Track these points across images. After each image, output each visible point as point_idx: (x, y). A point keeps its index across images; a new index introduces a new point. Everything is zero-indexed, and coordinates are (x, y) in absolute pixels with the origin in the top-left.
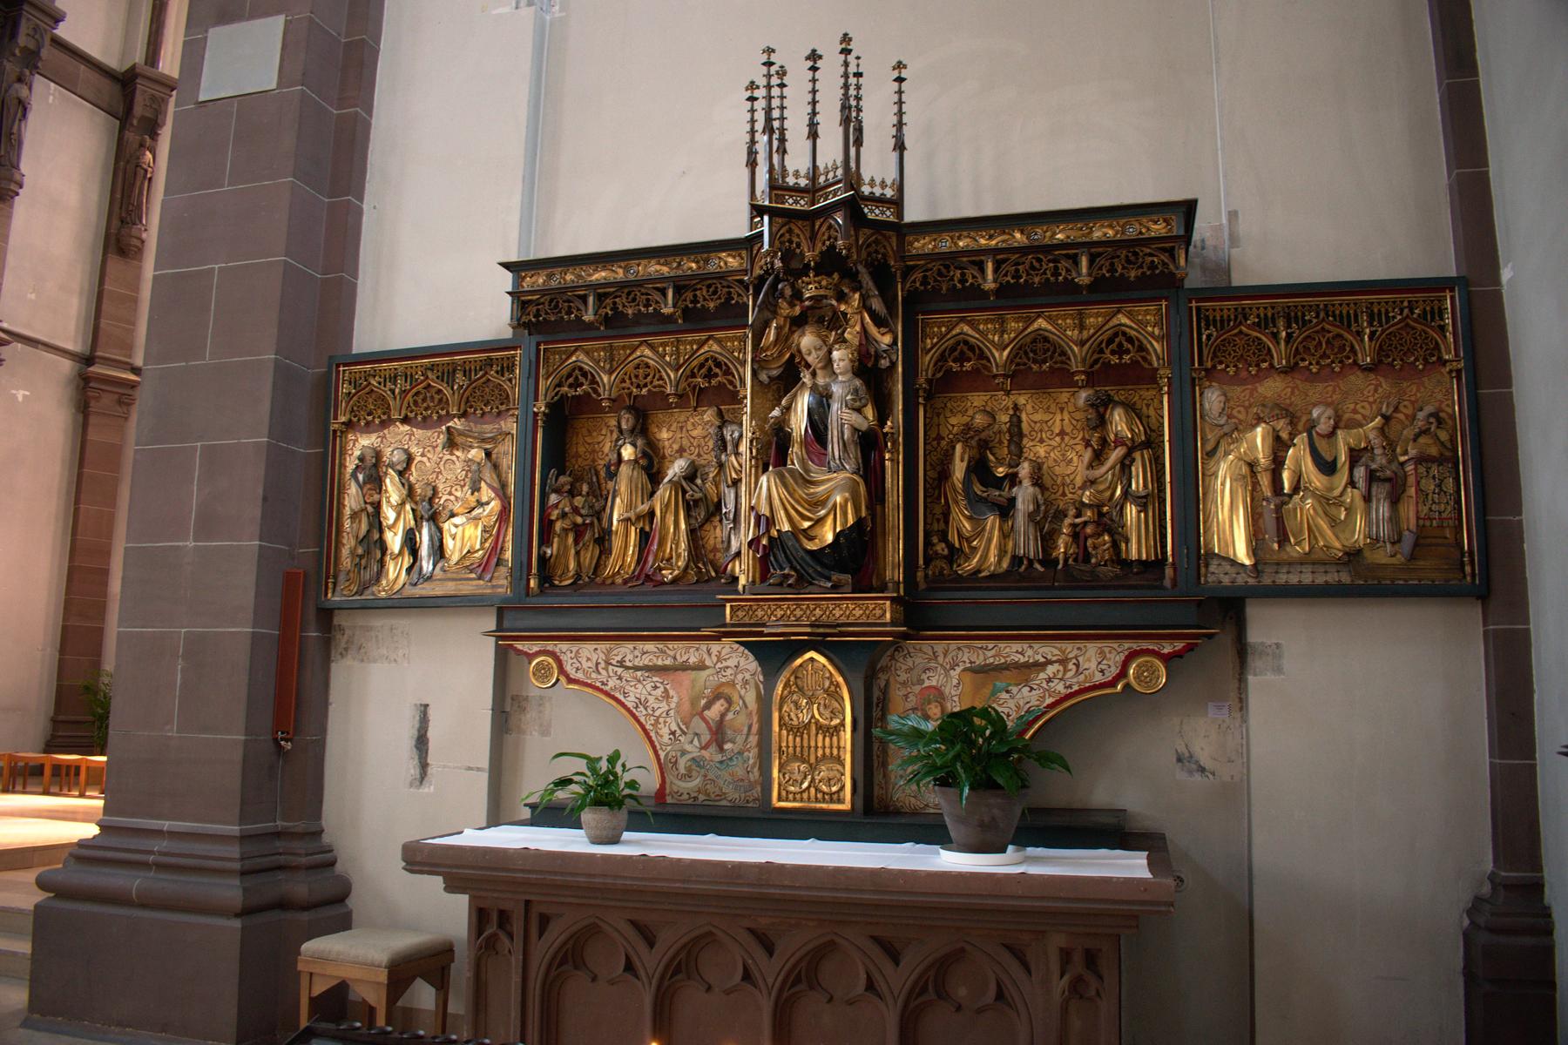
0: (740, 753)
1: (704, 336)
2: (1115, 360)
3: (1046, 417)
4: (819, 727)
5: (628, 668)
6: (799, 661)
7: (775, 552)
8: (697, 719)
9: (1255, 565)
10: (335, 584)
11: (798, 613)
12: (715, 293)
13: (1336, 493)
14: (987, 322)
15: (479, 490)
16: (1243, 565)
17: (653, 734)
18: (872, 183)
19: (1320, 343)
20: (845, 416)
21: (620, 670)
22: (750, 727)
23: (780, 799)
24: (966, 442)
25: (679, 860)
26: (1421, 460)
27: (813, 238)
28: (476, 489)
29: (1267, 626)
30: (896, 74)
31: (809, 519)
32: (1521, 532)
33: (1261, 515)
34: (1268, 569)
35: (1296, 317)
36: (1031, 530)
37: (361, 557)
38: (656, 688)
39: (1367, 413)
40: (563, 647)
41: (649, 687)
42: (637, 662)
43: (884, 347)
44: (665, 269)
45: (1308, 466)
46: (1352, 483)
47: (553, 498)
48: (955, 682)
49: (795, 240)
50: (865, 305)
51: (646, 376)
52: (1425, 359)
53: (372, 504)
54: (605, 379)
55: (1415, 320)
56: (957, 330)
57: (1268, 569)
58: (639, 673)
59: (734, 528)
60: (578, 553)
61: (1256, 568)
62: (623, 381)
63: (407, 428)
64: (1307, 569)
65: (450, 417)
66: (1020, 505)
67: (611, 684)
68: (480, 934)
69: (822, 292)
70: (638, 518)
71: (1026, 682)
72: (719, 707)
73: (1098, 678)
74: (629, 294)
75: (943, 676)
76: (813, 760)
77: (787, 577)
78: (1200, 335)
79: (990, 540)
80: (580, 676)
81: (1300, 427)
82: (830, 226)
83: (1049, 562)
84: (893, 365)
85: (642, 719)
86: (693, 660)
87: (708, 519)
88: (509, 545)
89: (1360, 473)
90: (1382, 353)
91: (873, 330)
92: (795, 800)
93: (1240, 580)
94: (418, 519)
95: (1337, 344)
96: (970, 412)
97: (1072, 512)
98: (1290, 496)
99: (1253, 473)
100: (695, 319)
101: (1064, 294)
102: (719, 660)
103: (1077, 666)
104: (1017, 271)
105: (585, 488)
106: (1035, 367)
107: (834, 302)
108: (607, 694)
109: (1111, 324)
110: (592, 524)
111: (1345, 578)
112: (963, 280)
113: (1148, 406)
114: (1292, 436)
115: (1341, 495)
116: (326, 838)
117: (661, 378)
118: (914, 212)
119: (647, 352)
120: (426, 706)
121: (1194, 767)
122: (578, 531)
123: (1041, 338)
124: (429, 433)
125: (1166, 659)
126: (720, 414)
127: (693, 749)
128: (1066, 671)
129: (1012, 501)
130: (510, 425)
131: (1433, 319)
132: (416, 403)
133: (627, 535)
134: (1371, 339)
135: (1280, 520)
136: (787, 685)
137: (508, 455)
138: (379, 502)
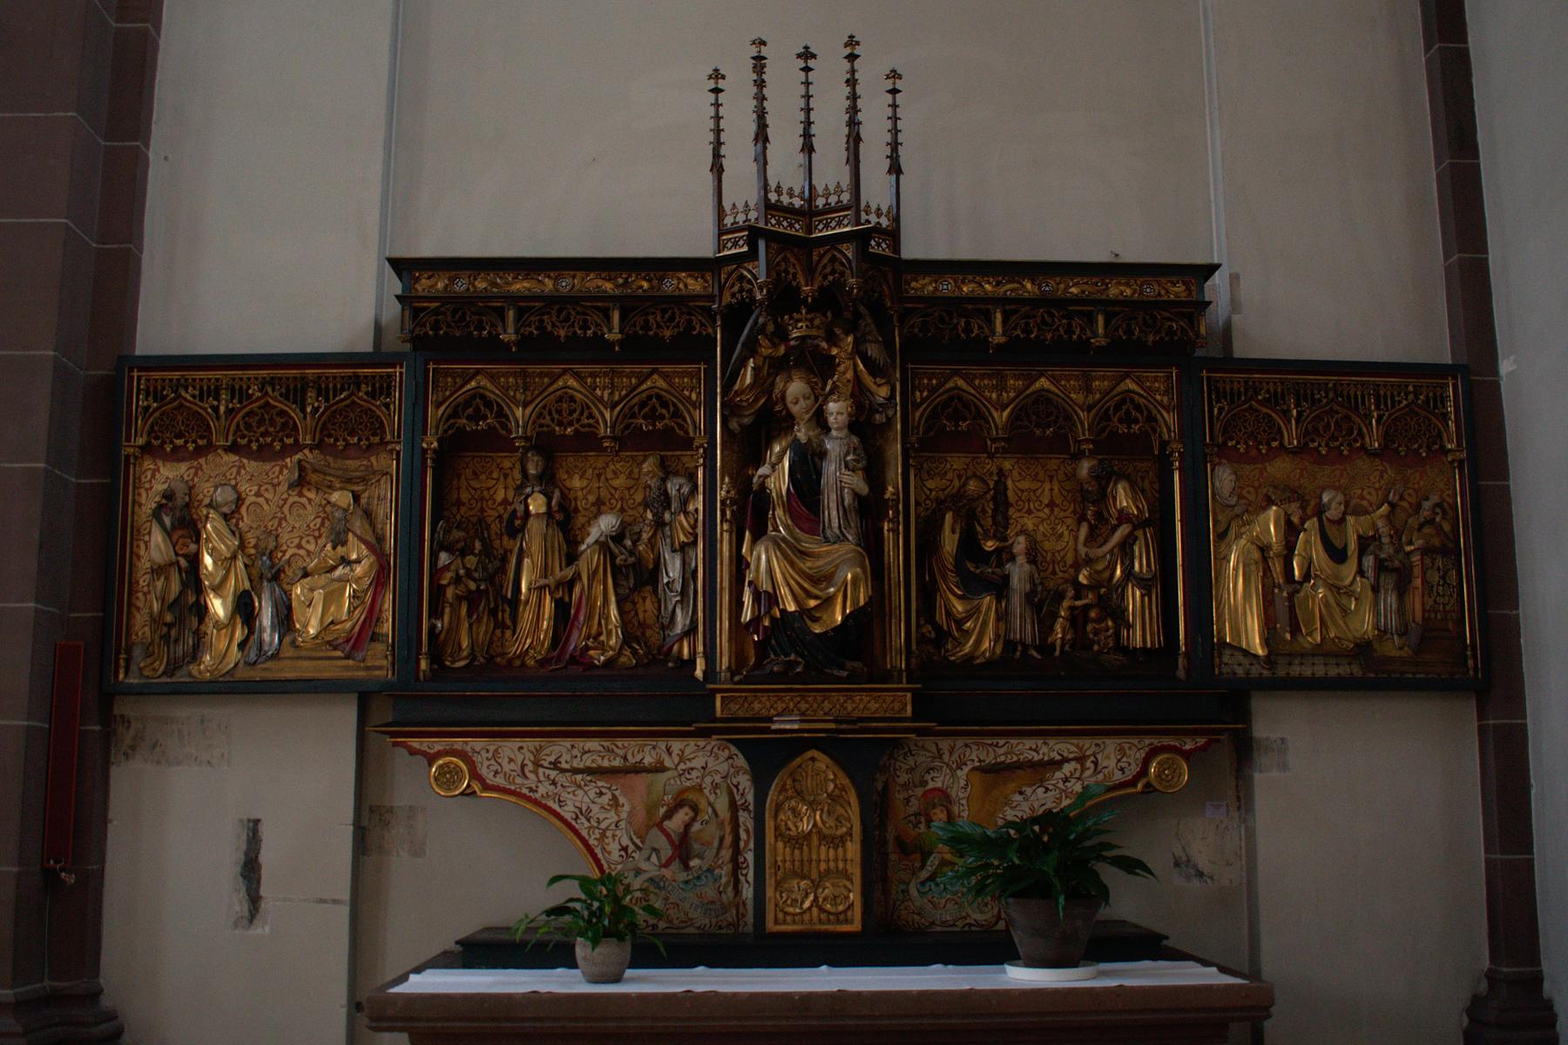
0: (710, 870)
1: (646, 368)
2: (1123, 429)
3: (1034, 486)
4: (823, 838)
5: (563, 771)
6: (799, 760)
8: (655, 830)
10: (128, 661)
11: (804, 706)
12: (672, 319)
13: (1347, 582)
14: (983, 377)
15: (344, 543)
16: (1256, 656)
17: (598, 851)
18: (827, 195)
20: (846, 479)
21: (553, 774)
22: (722, 839)
23: (776, 922)
24: (956, 512)
25: (735, 994)
26: (1426, 551)
27: (810, 271)
28: (340, 541)
29: (1272, 721)
30: (889, 85)
31: (816, 597)
32: (1518, 624)
35: (1305, 395)
36: (1028, 613)
37: (170, 626)
38: (601, 794)
39: (1373, 499)
40: (478, 743)
41: (592, 794)
43: (881, 400)
44: (608, 286)
45: (1318, 554)
46: (1361, 572)
47: (444, 558)
48: (962, 783)
49: (791, 270)
50: (859, 351)
51: (571, 412)
52: (1429, 447)
53: (185, 556)
54: (519, 412)
55: (1419, 407)
56: (950, 384)
58: (579, 777)
59: (681, 602)
60: (471, 625)
61: (1269, 660)
62: (540, 415)
63: (233, 458)
65: (298, 447)
67: (542, 790)
69: (814, 332)
70: (559, 584)
71: (1041, 782)
72: (682, 816)
73: (1118, 777)
74: (560, 311)
75: (955, 778)
76: (814, 875)
78: (1211, 412)
79: (985, 623)
80: (500, 781)
81: (1309, 511)
82: (833, 260)
83: (1045, 648)
84: (890, 421)
85: (584, 833)
86: (648, 760)
87: (636, 588)
89: (1369, 562)
90: (1387, 438)
91: (868, 380)
92: (794, 922)
93: (1255, 671)
94: (256, 581)
96: (950, 476)
97: (1071, 593)
99: (1265, 559)
100: (639, 349)
101: (1078, 355)
102: (682, 759)
103: (1096, 763)
105: (478, 545)
107: (824, 345)
108: (536, 803)
109: (1118, 389)
110: (487, 590)
111: (1357, 671)
112: (968, 330)
113: (1143, 478)
115: (1352, 584)
116: (106, 1002)
117: (591, 416)
118: (913, 248)
119: (572, 382)
120: (257, 822)
121: (1192, 871)
122: (473, 599)
123: (1042, 397)
124: (268, 466)
125: (1186, 755)
126: (663, 464)
127: (651, 868)
128: (1083, 769)
129: (1006, 578)
130: (381, 461)
131: (1436, 407)
132: (248, 427)
133: (540, 605)
134: (1378, 422)
135: (1292, 608)
136: (783, 789)
137: (385, 499)
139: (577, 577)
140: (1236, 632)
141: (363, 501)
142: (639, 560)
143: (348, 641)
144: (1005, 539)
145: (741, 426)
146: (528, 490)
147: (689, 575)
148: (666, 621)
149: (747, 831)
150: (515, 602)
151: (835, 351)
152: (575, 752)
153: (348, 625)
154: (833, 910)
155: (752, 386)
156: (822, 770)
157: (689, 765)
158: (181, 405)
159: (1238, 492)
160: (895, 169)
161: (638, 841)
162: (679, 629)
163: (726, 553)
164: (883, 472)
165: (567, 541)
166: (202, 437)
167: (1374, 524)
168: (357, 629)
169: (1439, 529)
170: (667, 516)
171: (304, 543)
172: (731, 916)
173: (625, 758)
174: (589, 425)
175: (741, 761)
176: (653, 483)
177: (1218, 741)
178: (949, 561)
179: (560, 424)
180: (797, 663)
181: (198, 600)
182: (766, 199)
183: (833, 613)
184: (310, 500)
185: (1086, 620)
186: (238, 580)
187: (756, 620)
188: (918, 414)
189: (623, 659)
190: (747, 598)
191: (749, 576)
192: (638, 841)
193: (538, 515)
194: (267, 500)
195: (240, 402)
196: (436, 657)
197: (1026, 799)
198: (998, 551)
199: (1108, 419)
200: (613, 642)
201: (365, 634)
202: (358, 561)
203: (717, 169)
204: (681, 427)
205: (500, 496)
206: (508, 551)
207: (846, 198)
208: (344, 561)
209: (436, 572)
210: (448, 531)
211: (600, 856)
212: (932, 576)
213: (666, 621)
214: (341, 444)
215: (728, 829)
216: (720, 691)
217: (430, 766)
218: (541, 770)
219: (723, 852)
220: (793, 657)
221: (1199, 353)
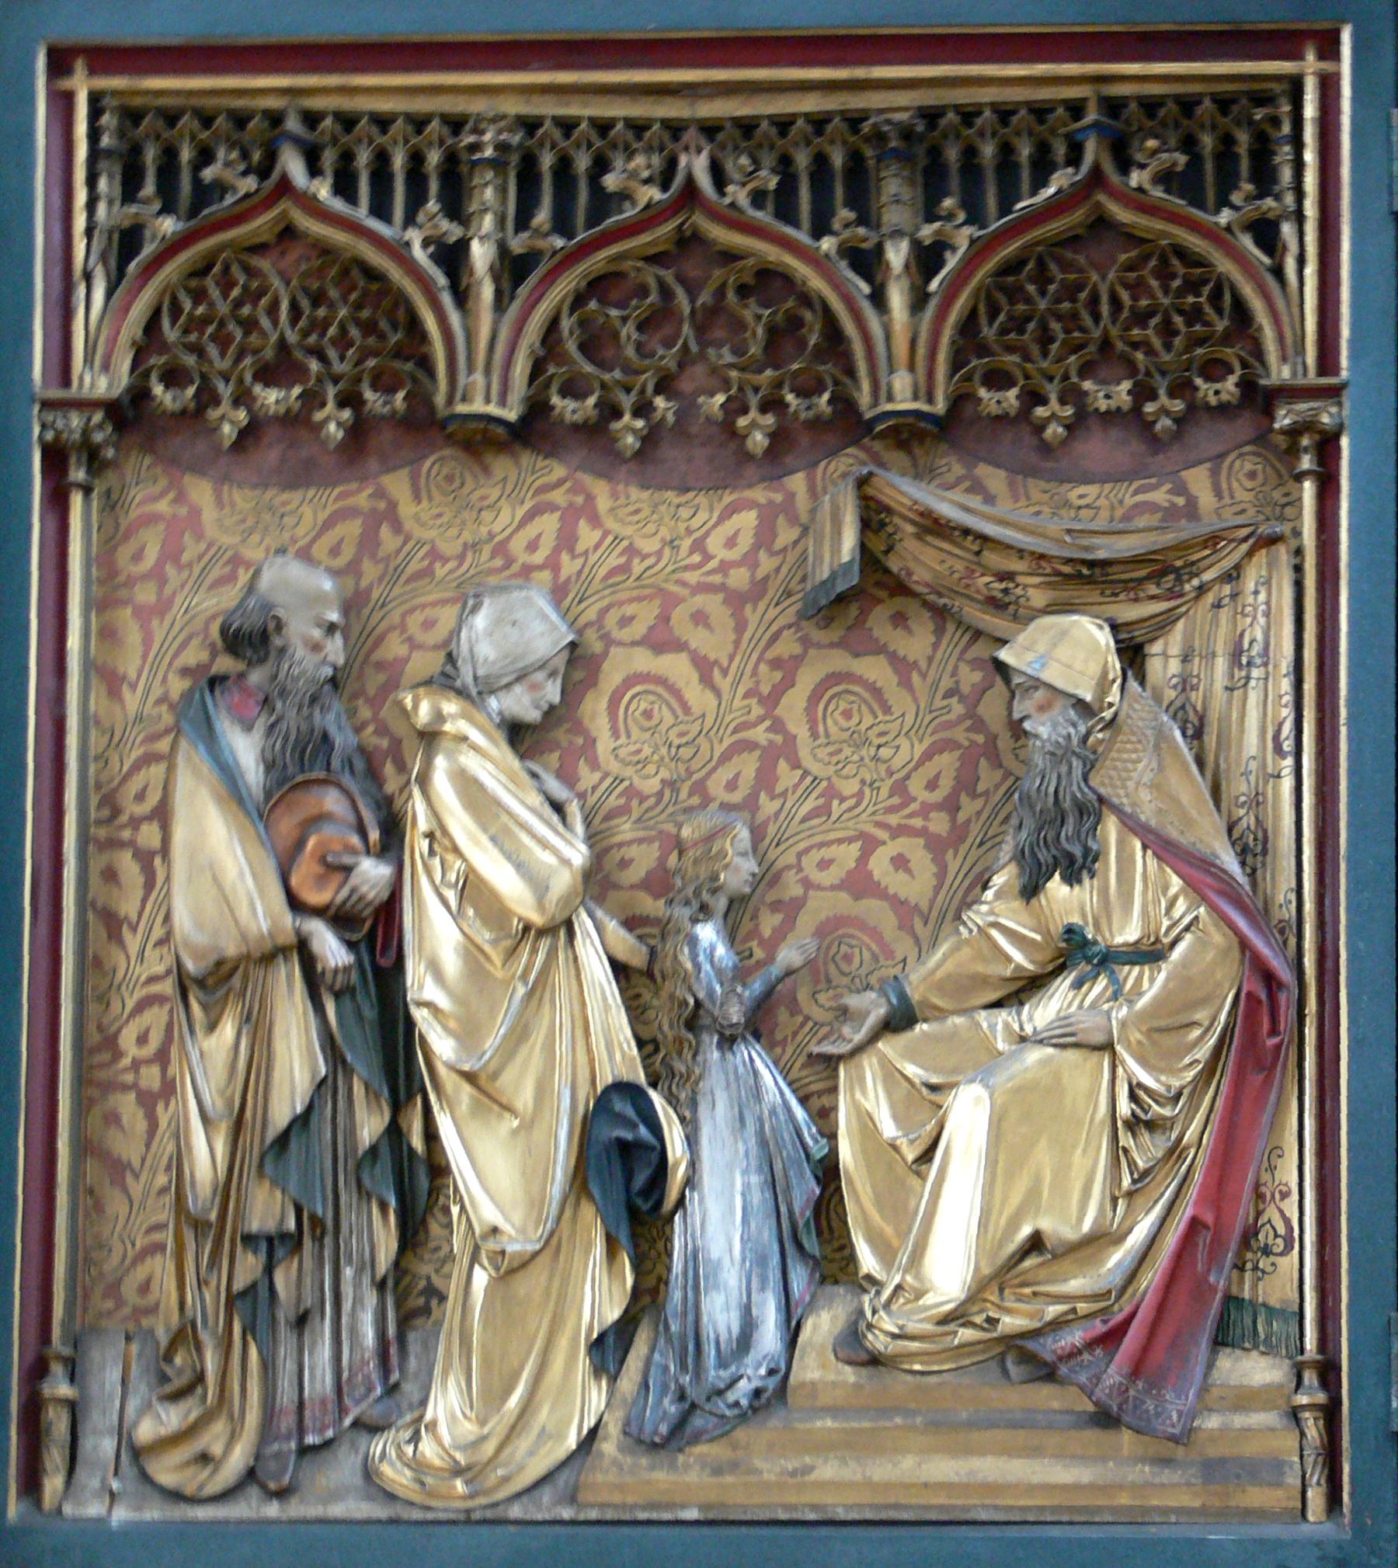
37: (274, 1246)
53: (341, 919)
88: (1293, 1205)
94: (671, 1025)
138: (389, 911)
143: (1112, 1338)
158: (288, 233)
166: (385, 383)
168: (1150, 1279)
171: (880, 865)
184: (902, 667)
194: (705, 668)
201: (1202, 1293)
202: (1149, 953)
214: (1053, 411)
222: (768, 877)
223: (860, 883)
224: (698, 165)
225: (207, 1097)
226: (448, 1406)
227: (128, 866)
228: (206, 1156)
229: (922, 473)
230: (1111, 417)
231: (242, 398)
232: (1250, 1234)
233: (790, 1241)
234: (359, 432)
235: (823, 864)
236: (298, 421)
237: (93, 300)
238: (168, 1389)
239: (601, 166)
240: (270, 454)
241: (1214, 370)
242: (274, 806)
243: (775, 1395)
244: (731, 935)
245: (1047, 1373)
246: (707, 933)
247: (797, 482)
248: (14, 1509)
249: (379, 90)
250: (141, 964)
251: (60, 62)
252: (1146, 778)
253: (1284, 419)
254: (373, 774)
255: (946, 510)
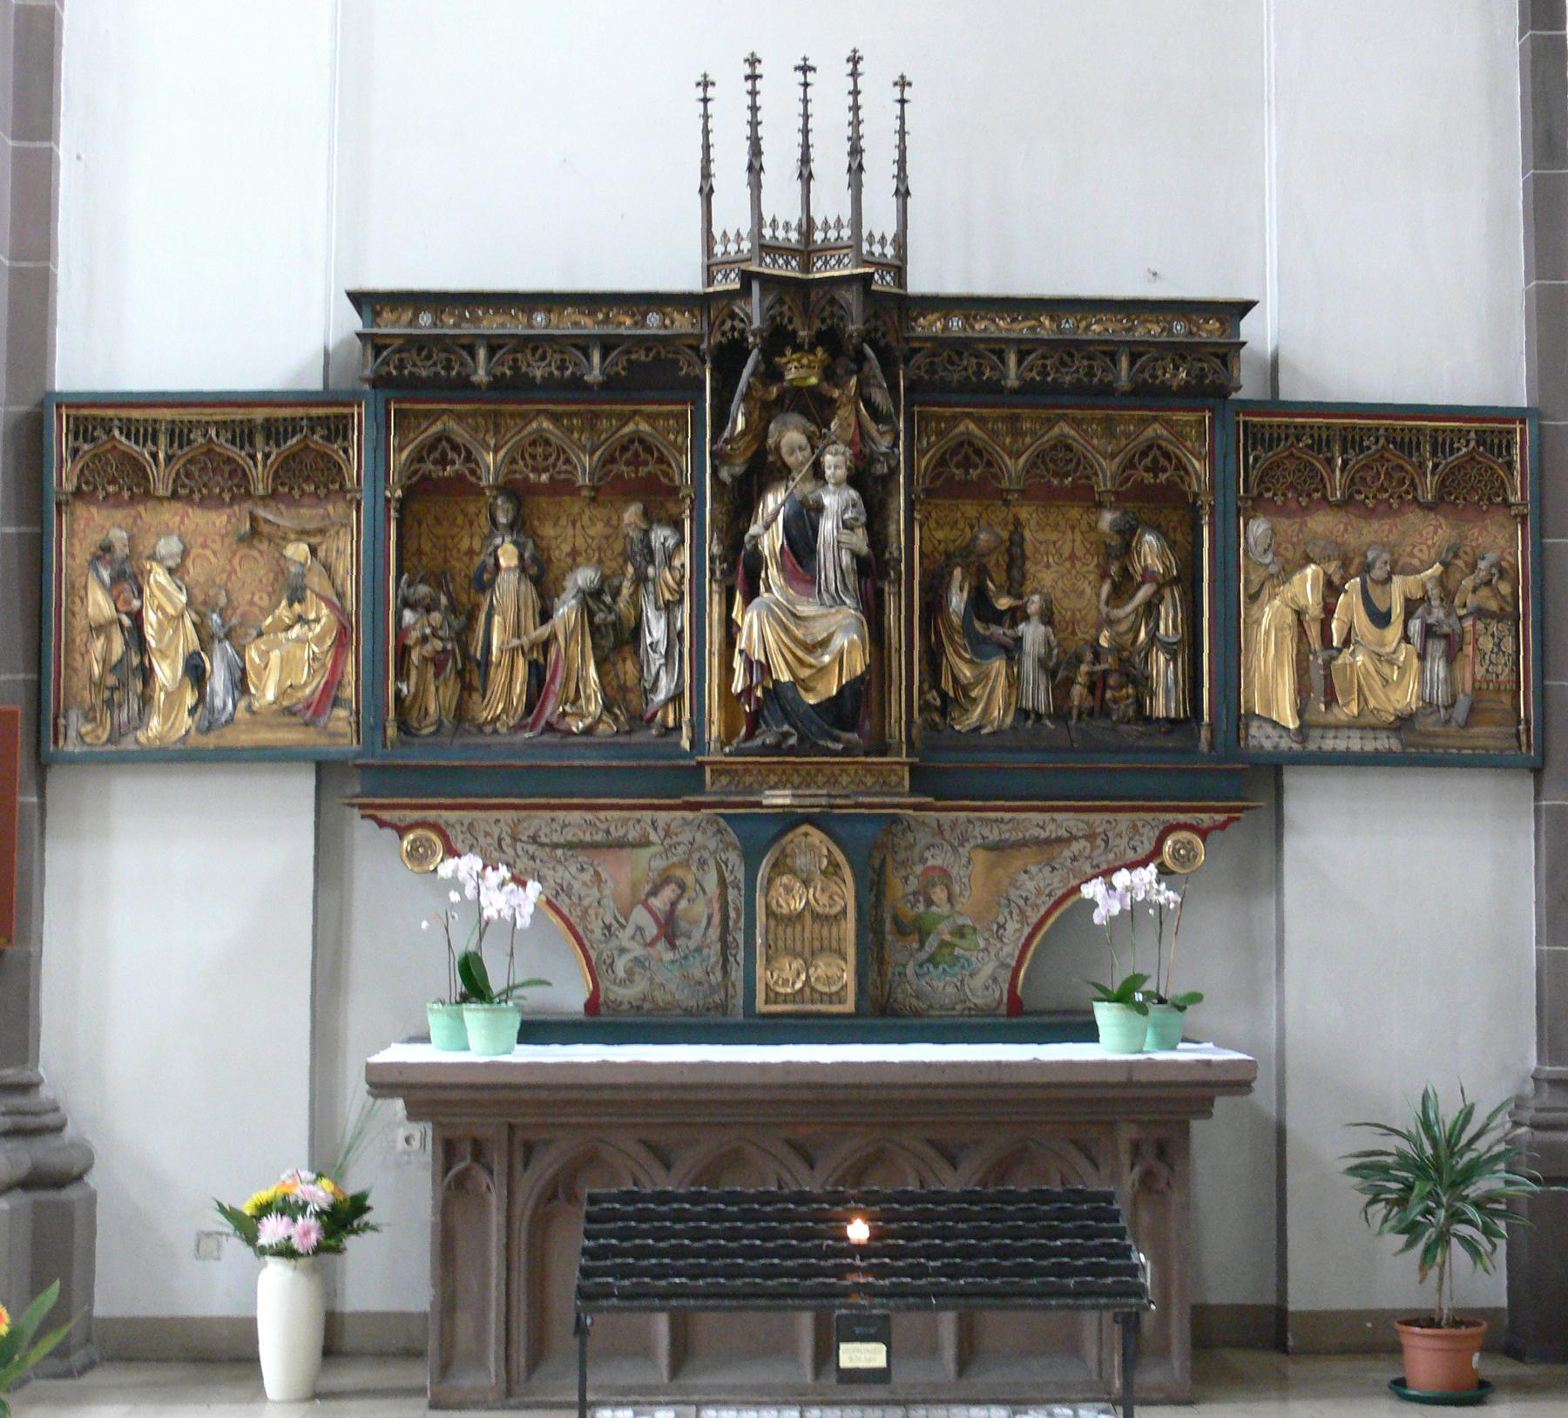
0: (699, 950)
3: (1054, 536)
4: (816, 917)
5: (542, 845)
7: (769, 703)
8: (640, 907)
9: (1300, 729)
13: (1389, 649)
16: (1286, 729)
19: (1378, 474)
21: (532, 848)
22: (710, 918)
23: (767, 1002)
24: (966, 569)
27: (806, 312)
33: (1307, 670)
34: (1315, 733)
35: (1353, 440)
37: (113, 689)
38: (583, 869)
39: (1425, 557)
41: (573, 869)
42: (556, 838)
43: (883, 449)
46: (1406, 638)
51: (546, 458)
52: (1490, 499)
53: (128, 614)
54: (490, 458)
57: (1315, 733)
58: (559, 852)
61: (1303, 731)
64: (1356, 734)
66: (1028, 645)
68: (447, 1169)
70: (533, 646)
72: (669, 893)
77: (786, 735)
81: (1352, 571)
84: (894, 471)
85: (565, 911)
86: (633, 835)
88: (350, 676)
89: (1415, 626)
91: (872, 427)
93: (1285, 744)
94: (206, 639)
95: (1397, 475)
96: (961, 525)
97: (1089, 656)
98: (1340, 651)
99: (1300, 623)
103: (1106, 842)
104: (1044, 366)
105: (444, 600)
106: (1055, 482)
114: (1345, 580)
117: (568, 461)
118: (920, 282)
125: (1204, 834)
129: (1019, 640)
135: (1328, 679)
137: (344, 551)
138: (140, 612)
139: (553, 637)
140: (1267, 705)
141: (321, 553)
142: (619, 618)
143: (309, 707)
144: (1020, 596)
145: (732, 476)
146: (498, 541)
147: (674, 636)
148: (648, 686)
149: (737, 910)
150: (485, 664)
151: (836, 393)
152: (555, 826)
153: (308, 691)
154: (826, 990)
155: (743, 433)
156: (813, 845)
157: (675, 839)
158: (115, 447)
159: (1273, 547)
160: (903, 194)
161: (622, 920)
162: (661, 696)
163: (716, 616)
164: (886, 527)
165: (541, 596)
166: (138, 485)
167: (1424, 586)
168: (317, 695)
169: (1497, 593)
170: (651, 571)
171: (256, 599)
172: (718, 998)
173: (608, 832)
174: (566, 472)
175: (732, 837)
176: (635, 535)
177: (1238, 819)
178: (956, 620)
179: (534, 470)
180: (792, 735)
181: (142, 662)
182: (761, 236)
183: (830, 683)
184: (261, 552)
185: (1105, 686)
186: (188, 638)
187: (748, 690)
188: (923, 463)
189: (601, 727)
190: (738, 663)
191: (742, 643)
192: (622, 920)
193: (509, 569)
194: (215, 553)
195: (181, 447)
196: (403, 726)
197: (1032, 879)
198: (1012, 610)
199: (1134, 468)
200: (592, 708)
201: (330, 695)
202: (317, 620)
203: (707, 193)
204: (666, 475)
205: (465, 545)
206: (476, 607)
207: (846, 233)
208: (300, 619)
209: (401, 631)
210: (410, 584)
211: (581, 933)
212: (938, 633)
213: (648, 686)
214: (296, 493)
215: (716, 906)
216: (710, 763)
217: (401, 838)
218: (519, 845)
219: (711, 931)
220: (786, 728)
221: (1234, 396)
222: (229, 601)
223: (251, 603)
224: (213, 432)
225: (98, 655)
226: (155, 723)
227: (77, 600)
228: (96, 670)
229: (265, 506)
230: (310, 494)
231: (104, 488)
232: (340, 683)
233: (234, 686)
234: (132, 497)
235: (242, 599)
236: (118, 494)
237: (67, 466)
238: (59, 440)
239: (190, 431)
240: (111, 501)
241: (333, 482)
242: (112, 589)
243: (231, 720)
244: (220, 616)
245: (294, 714)
246: (215, 617)
247: (236, 508)
248: (52, 748)
249: (136, 414)
250: (80, 623)
251: (59, 406)
252: (316, 581)
253: (348, 497)
254: (136, 577)
255: (270, 517)
